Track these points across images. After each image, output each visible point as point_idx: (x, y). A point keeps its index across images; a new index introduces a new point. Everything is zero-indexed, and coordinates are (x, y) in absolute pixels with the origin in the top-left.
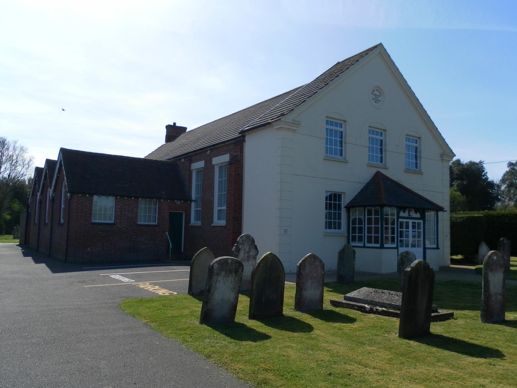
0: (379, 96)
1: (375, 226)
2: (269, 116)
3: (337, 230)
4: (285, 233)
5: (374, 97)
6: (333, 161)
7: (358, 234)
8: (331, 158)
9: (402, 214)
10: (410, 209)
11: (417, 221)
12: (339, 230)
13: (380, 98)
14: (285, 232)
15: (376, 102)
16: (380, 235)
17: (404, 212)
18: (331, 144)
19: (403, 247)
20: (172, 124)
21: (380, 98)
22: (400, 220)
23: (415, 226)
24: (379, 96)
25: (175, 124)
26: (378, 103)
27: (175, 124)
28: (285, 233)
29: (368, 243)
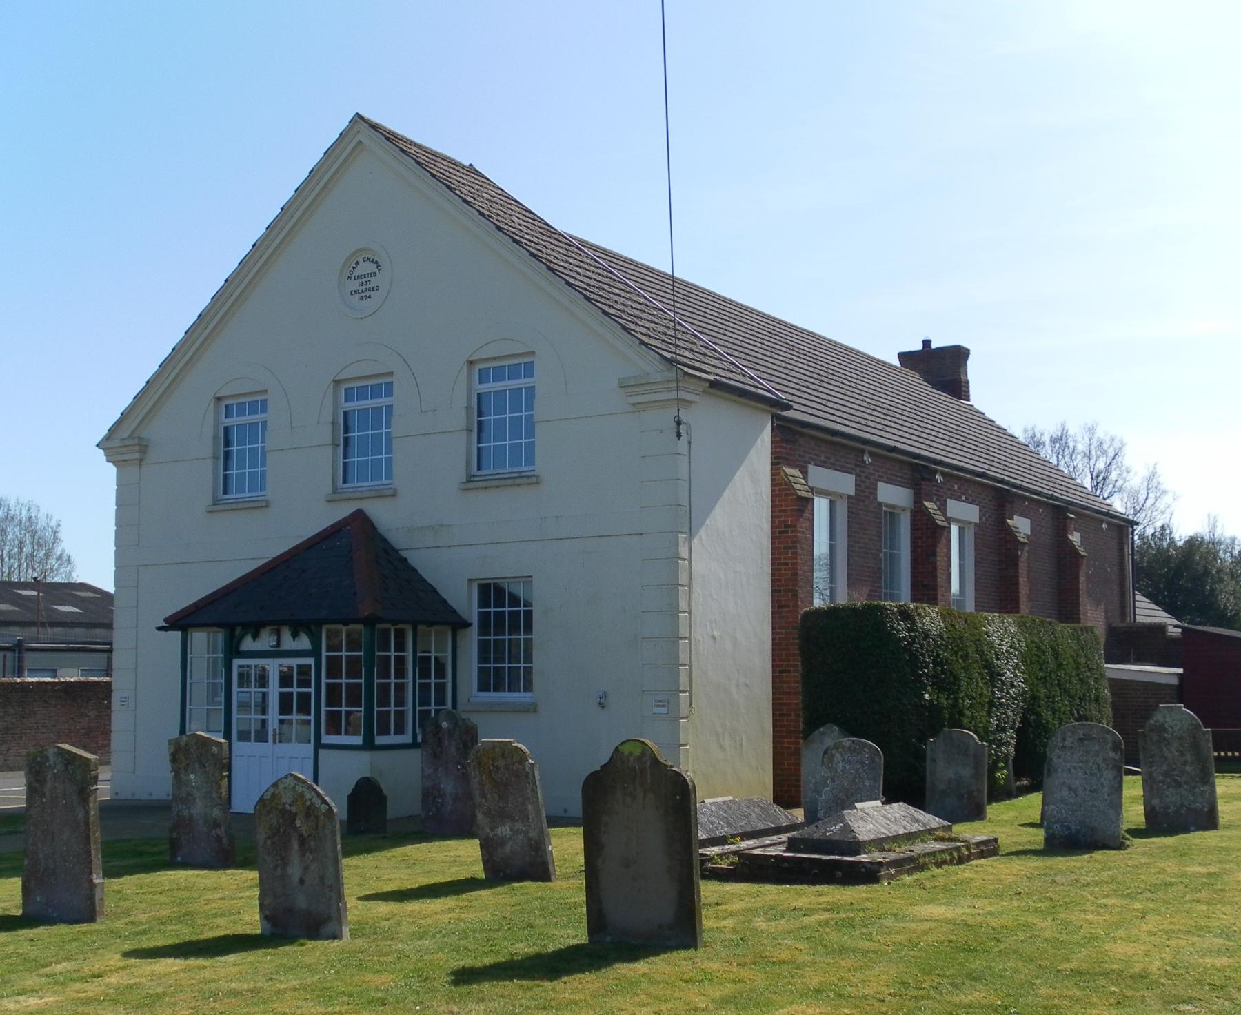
0: (373, 275)
1: (388, 681)
2: (696, 320)
3: (492, 694)
4: (661, 701)
5: (354, 285)
6: (224, 510)
7: (395, 706)
8: (232, 503)
9: (248, 644)
10: (277, 626)
11: (295, 662)
12: (528, 694)
13: (374, 282)
14: (662, 704)
15: (362, 298)
16: (376, 709)
17: (255, 636)
18: (516, 422)
19: (337, 734)
20: (919, 347)
21: (374, 282)
22: (237, 662)
23: (248, 675)
24: (373, 275)
25: (927, 343)
26: (370, 297)
27: (927, 343)
28: (661, 701)
29: (328, 733)
